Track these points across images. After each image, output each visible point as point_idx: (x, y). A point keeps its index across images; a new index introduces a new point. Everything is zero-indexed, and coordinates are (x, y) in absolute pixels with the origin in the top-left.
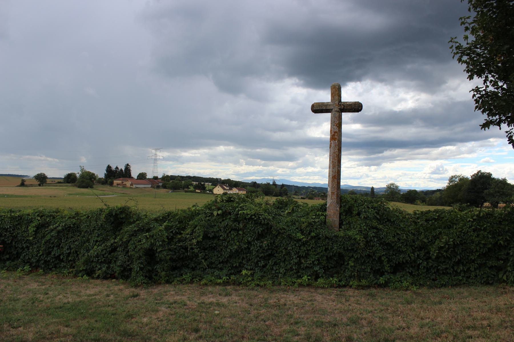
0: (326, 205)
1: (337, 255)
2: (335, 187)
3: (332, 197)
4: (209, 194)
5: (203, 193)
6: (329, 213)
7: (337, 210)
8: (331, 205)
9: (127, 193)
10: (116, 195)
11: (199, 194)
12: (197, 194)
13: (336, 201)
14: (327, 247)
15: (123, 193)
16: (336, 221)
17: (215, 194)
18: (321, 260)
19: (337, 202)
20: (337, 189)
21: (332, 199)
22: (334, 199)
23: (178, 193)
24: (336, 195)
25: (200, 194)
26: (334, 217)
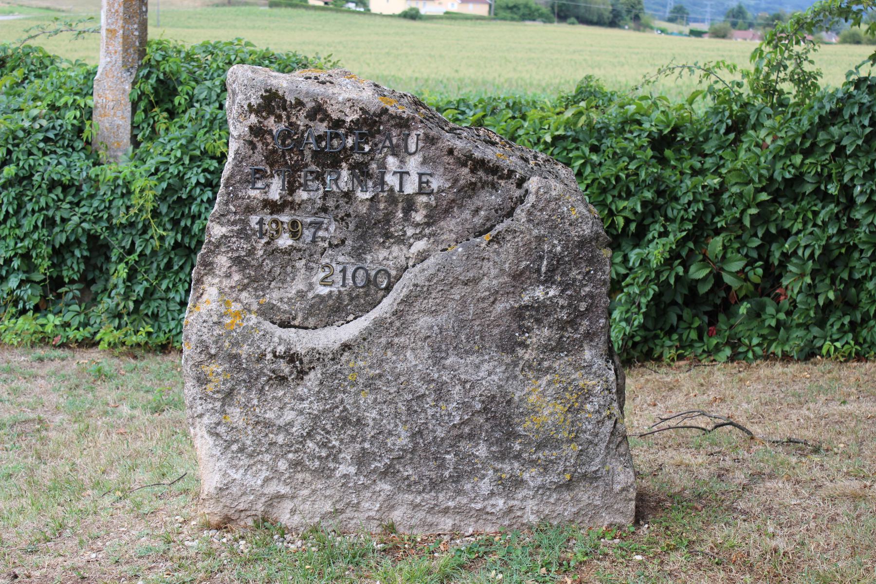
0: (95, 73)
1: (84, 240)
2: (117, 11)
3: (111, 48)
4: (354, 12)
5: (331, 10)
6: (100, 101)
7: (124, 91)
8: (106, 73)
9: (64, 8)
10: (20, 13)
11: (318, 13)
12: (311, 12)
13: (120, 63)
14: (50, 213)
15: (48, 9)
16: (122, 130)
17: (376, 15)
18: (34, 255)
19: (124, 64)
20: (125, 19)
21: (108, 52)
22: (116, 52)
23: (243, 8)
24: (121, 40)
25: (323, 13)
26: (115, 114)
